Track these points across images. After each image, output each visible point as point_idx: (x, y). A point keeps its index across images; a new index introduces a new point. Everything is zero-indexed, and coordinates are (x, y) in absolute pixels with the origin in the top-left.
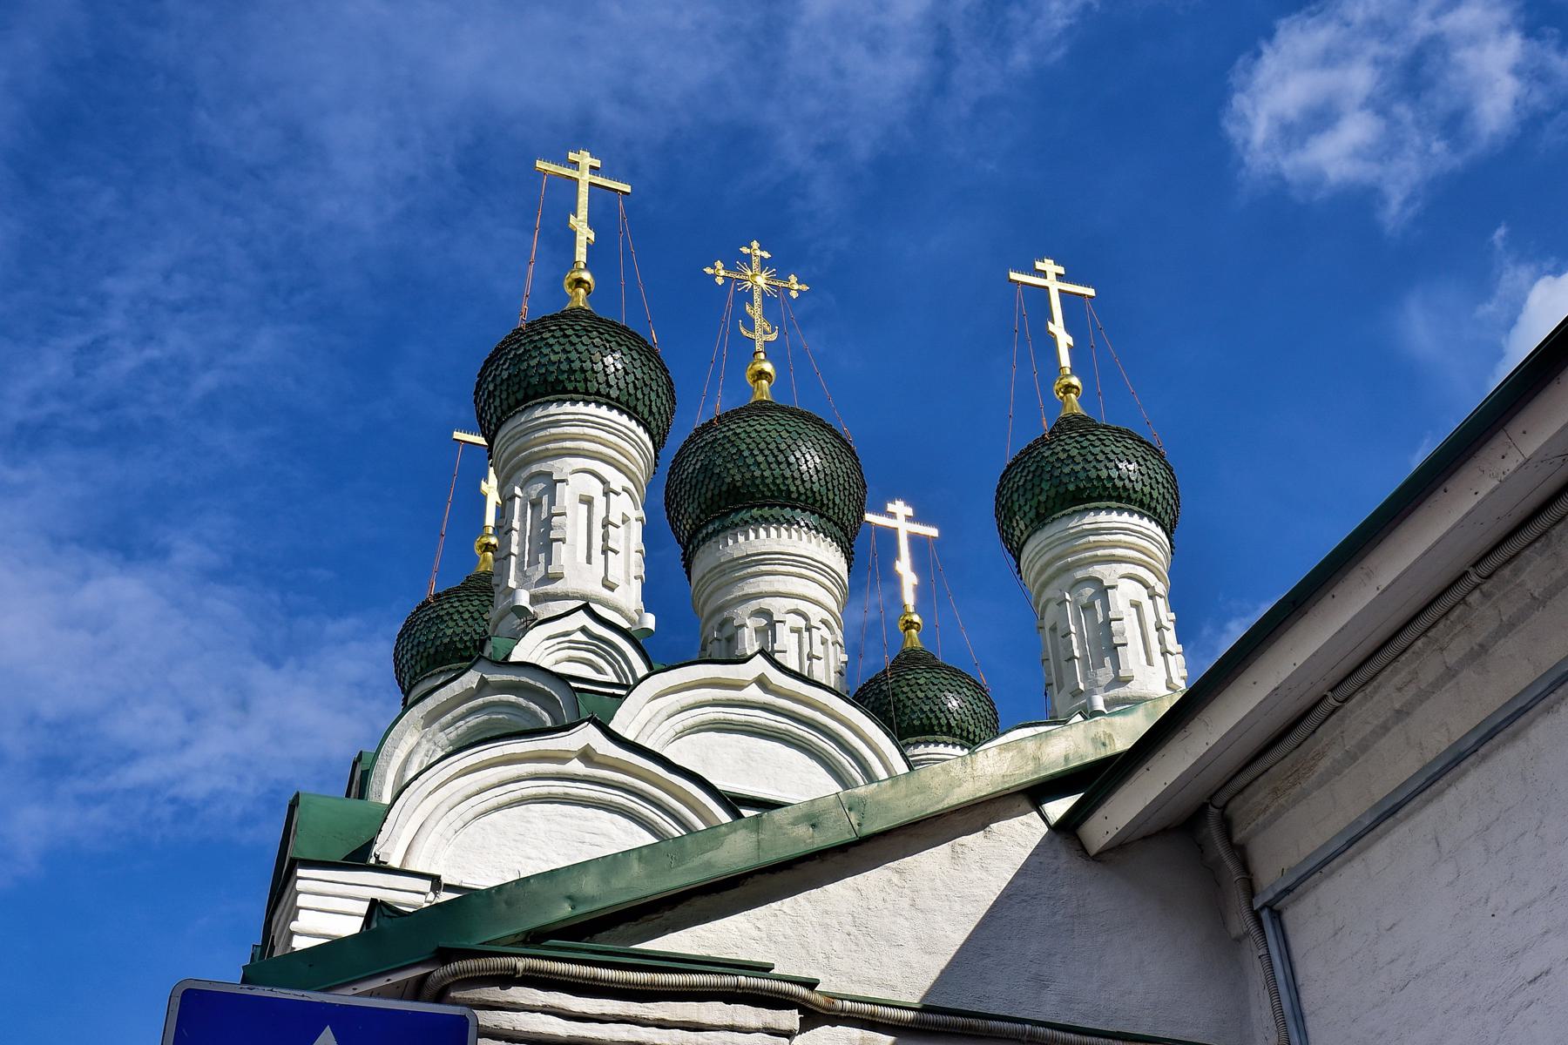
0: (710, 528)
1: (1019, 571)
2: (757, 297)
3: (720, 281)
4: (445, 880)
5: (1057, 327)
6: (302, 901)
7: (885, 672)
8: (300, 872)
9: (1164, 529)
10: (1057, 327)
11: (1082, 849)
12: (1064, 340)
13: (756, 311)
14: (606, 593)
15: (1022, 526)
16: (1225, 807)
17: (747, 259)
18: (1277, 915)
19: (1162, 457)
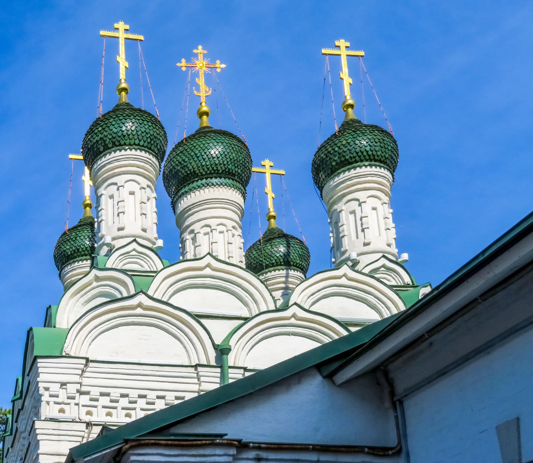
0: (183, 191)
1: (322, 197)
2: (201, 73)
3: (184, 69)
4: (90, 359)
5: (345, 74)
6: (40, 370)
7: (260, 241)
8: (39, 360)
9: (390, 172)
10: (345, 74)
11: (334, 383)
12: (347, 81)
13: (201, 81)
14: (143, 234)
15: (324, 176)
16: (386, 367)
17: (196, 55)
18: (401, 403)
19: (392, 137)
